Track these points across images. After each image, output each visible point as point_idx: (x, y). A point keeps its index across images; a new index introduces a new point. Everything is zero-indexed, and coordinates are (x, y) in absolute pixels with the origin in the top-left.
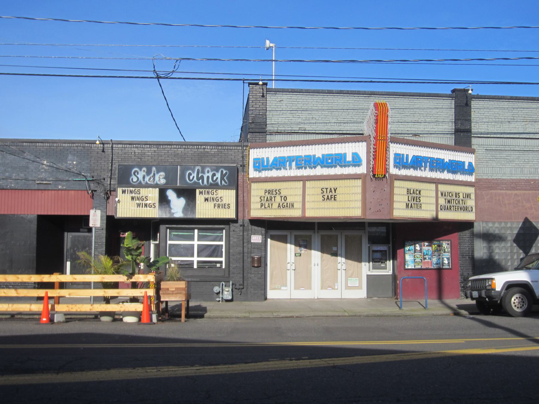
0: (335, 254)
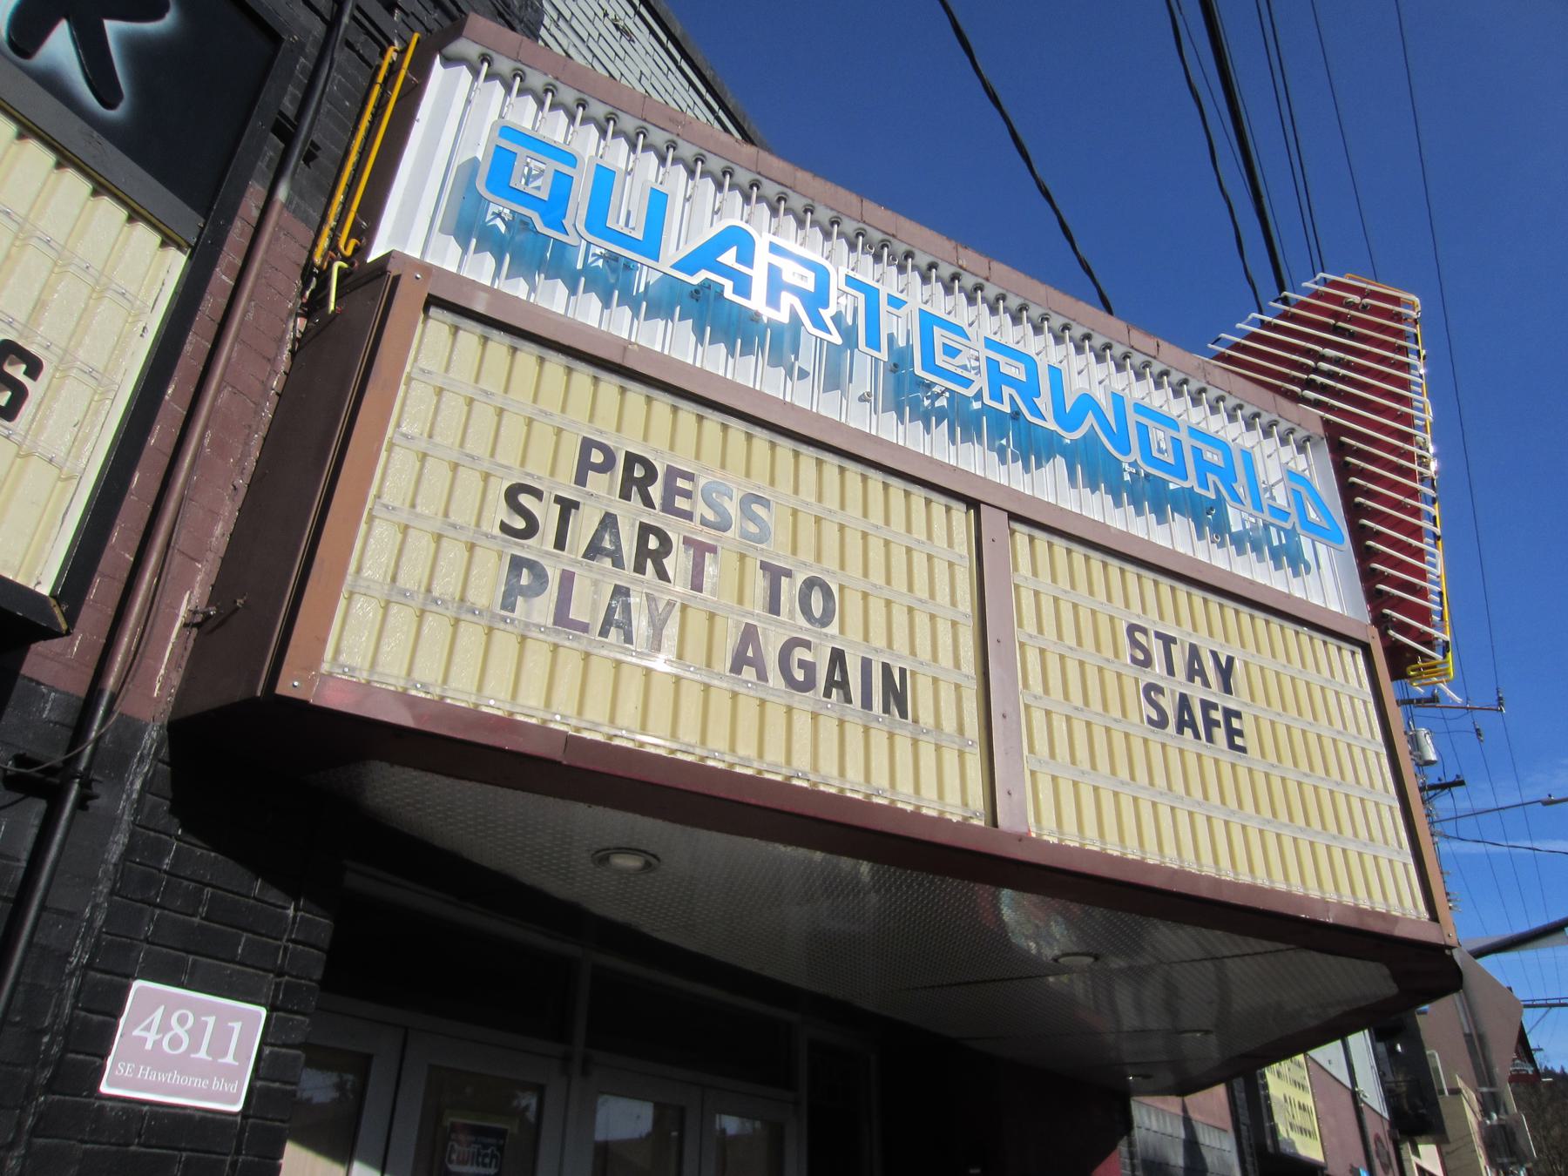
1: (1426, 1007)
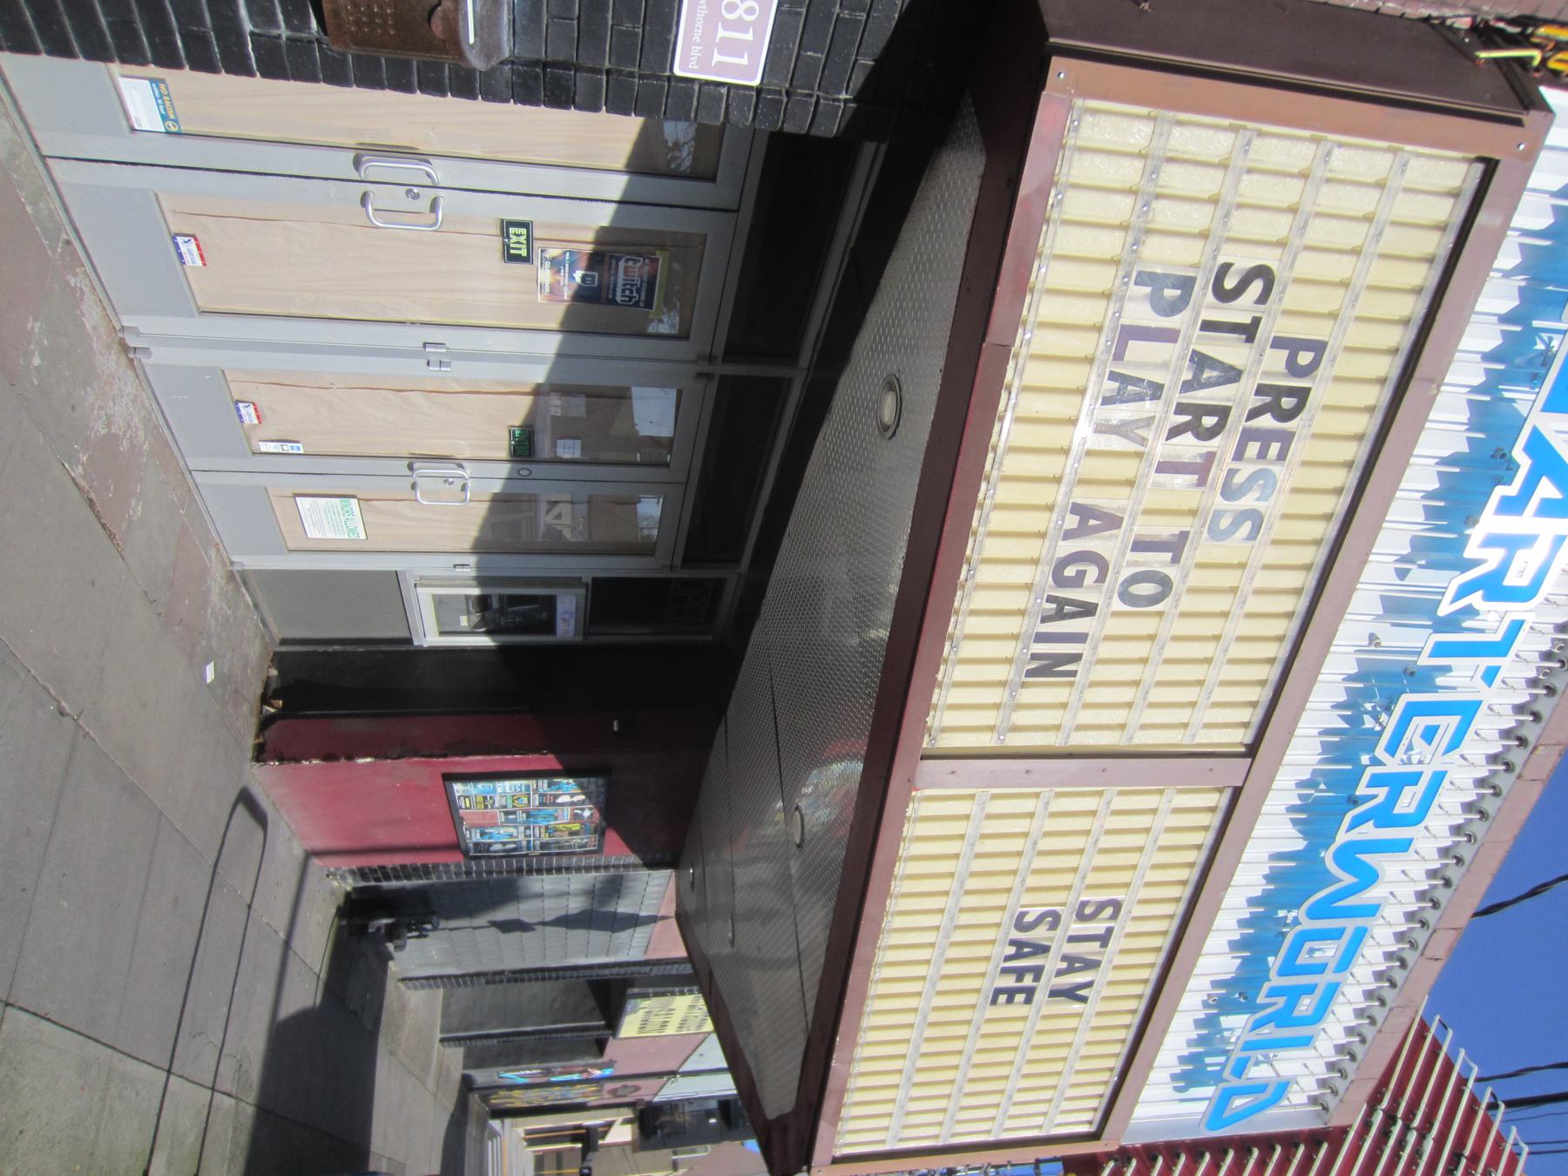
0: (524, 447)
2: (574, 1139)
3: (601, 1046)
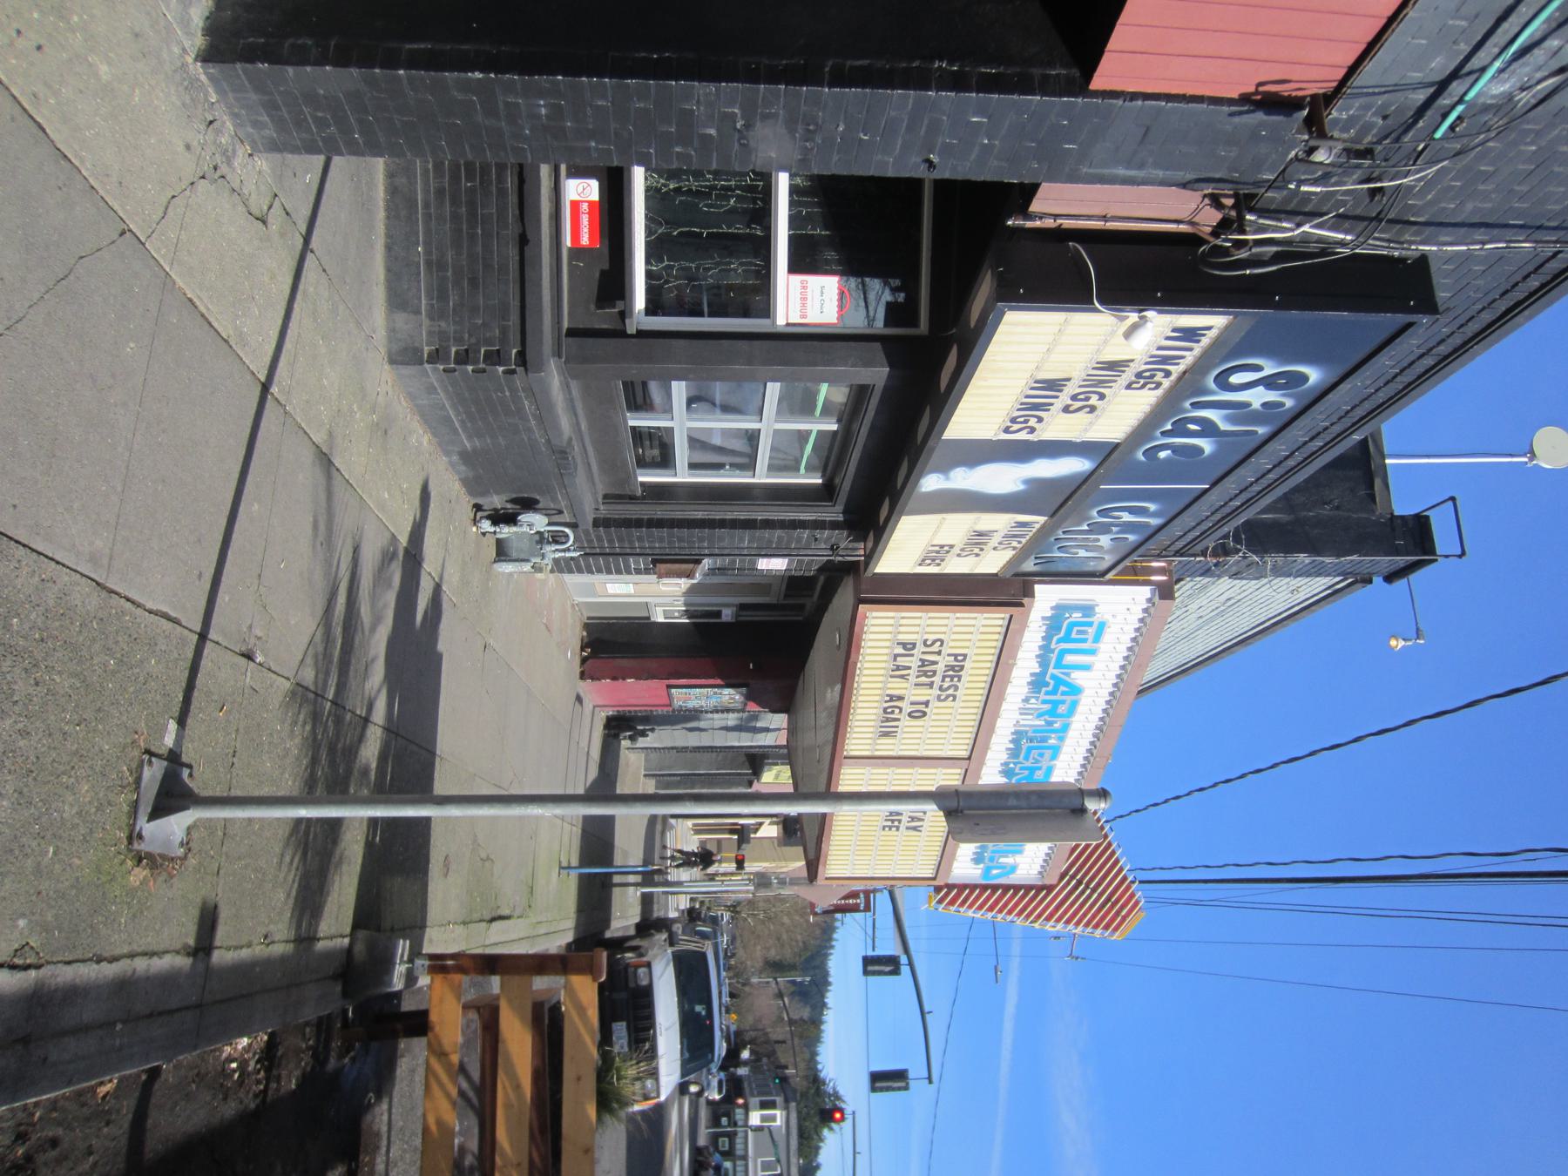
1: (150, 1121)
2: (732, 832)
3: (750, 784)
